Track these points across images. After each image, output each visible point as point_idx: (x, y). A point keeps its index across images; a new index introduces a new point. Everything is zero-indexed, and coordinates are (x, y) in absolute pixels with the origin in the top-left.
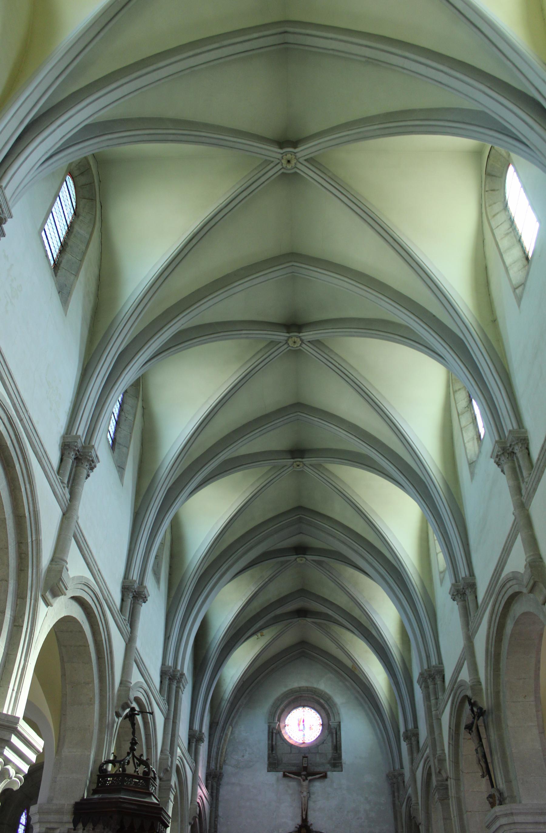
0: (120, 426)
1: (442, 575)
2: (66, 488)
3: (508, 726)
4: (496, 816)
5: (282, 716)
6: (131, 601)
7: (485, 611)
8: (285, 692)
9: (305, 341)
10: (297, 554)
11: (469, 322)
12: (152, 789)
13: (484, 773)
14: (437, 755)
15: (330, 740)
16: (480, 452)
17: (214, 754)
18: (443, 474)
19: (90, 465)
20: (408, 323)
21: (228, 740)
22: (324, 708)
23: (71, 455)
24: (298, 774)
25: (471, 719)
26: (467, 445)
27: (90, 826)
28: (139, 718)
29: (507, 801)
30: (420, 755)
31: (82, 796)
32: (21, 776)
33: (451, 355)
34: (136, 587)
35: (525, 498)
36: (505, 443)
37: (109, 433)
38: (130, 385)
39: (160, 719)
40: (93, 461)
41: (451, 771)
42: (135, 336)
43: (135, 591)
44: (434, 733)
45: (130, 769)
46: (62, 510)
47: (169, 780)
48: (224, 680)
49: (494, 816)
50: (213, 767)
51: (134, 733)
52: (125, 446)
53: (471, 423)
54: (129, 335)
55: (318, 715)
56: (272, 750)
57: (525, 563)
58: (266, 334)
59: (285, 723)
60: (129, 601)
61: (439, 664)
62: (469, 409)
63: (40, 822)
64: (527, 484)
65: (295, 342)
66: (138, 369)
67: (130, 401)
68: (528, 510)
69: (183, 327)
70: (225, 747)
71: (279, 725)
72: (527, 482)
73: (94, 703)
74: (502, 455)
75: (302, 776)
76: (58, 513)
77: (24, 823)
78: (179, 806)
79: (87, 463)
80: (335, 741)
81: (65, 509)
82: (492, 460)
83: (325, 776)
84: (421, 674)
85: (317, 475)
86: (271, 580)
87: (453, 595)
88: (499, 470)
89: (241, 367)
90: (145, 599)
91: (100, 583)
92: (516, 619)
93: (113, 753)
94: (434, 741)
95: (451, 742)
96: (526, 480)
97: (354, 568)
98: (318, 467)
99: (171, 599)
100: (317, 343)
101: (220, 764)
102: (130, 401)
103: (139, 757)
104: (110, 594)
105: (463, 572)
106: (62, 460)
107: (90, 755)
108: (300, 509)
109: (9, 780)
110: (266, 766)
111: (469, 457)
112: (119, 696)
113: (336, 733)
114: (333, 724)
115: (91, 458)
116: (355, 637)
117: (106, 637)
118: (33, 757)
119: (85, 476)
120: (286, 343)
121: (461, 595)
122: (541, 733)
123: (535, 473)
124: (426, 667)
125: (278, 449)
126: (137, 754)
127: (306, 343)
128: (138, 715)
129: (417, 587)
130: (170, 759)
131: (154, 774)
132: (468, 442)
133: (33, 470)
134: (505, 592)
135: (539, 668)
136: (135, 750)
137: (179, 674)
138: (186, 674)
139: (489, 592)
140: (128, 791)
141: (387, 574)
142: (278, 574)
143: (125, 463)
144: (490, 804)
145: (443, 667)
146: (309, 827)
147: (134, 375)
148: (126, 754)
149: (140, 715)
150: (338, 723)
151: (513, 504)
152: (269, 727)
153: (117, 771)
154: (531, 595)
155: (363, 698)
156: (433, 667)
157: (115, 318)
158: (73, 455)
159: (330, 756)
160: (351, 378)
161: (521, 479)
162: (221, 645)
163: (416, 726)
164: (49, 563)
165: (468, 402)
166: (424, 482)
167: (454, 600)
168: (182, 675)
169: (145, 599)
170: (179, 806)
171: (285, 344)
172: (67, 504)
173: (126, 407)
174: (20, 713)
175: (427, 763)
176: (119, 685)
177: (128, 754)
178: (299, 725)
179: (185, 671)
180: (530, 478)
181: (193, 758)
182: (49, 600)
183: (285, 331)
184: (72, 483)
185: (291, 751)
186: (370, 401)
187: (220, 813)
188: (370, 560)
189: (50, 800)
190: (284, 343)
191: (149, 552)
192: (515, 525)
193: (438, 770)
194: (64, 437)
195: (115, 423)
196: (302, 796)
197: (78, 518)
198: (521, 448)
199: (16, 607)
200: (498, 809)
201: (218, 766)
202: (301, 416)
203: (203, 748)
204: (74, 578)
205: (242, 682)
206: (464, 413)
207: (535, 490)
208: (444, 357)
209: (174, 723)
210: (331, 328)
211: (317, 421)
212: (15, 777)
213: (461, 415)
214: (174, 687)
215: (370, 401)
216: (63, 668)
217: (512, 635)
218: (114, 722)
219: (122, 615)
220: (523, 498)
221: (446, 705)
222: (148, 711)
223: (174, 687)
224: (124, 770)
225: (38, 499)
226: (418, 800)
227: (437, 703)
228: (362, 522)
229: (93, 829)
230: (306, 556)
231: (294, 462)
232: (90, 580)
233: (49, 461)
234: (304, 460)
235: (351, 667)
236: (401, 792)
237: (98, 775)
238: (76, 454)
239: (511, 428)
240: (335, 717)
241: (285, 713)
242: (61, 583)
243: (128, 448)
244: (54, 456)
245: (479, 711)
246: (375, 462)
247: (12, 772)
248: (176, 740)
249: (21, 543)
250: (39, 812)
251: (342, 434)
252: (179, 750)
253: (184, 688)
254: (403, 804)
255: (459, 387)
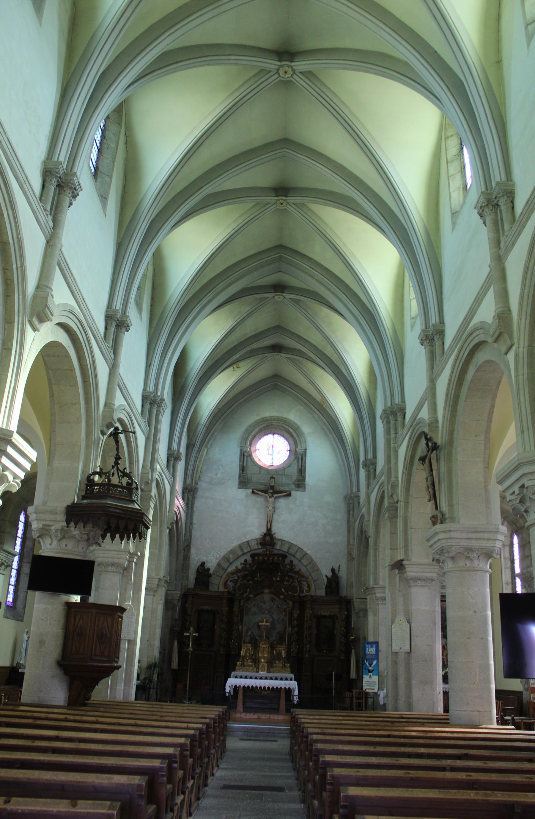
0: (102, 154)
1: (413, 320)
2: (49, 216)
3: (457, 460)
4: (436, 532)
5: (254, 441)
6: (115, 329)
7: (450, 356)
8: (257, 420)
9: (296, 72)
10: (275, 292)
11: (472, 61)
12: (135, 497)
13: (430, 497)
14: (391, 482)
15: (296, 465)
16: (464, 202)
17: (190, 471)
18: (425, 223)
19: (73, 193)
20: (407, 58)
21: (203, 460)
22: (292, 436)
23: (53, 182)
24: (266, 492)
25: (425, 453)
26: (452, 194)
27: (81, 525)
28: (122, 437)
29: (447, 521)
30: (376, 480)
31: (73, 501)
32: (19, 481)
33: (448, 98)
34: (119, 316)
35: (503, 251)
36: (491, 194)
37: (91, 161)
38: (113, 109)
39: (141, 439)
40: (75, 189)
41: (402, 495)
42: (117, 55)
43: (118, 320)
44: (390, 463)
45: (115, 480)
46: (45, 237)
47: (150, 491)
48: (201, 407)
49: (434, 532)
50: (189, 483)
51: (117, 449)
52: (107, 175)
53: (459, 172)
54: (110, 53)
55: (286, 442)
56: (243, 471)
57: (494, 314)
58: (256, 61)
59: (255, 448)
60: (112, 330)
61: (402, 403)
62: (459, 157)
63: (37, 520)
64: (506, 238)
65: (286, 72)
66: (121, 93)
67: (112, 128)
68: (504, 264)
69: (169, 48)
70: (201, 466)
71: (250, 449)
72: (507, 236)
73: (81, 422)
74: (486, 207)
75: (269, 494)
76: (41, 241)
77: (23, 521)
78: (158, 513)
79: (70, 190)
80: (300, 465)
81: (49, 237)
82: (476, 211)
83: (289, 495)
84: (384, 411)
85: (300, 215)
86: (249, 315)
87: (422, 340)
88: (482, 221)
89: (229, 96)
90: (128, 328)
91: (85, 311)
92: (478, 365)
93: (99, 466)
94: (390, 469)
95: (405, 471)
96: (506, 234)
97: (330, 308)
98: (301, 206)
99: (153, 330)
100: (308, 74)
101: (196, 481)
102: (112, 128)
103: (123, 471)
104: (94, 322)
105: (434, 319)
106: (43, 187)
107: (78, 467)
108: (281, 247)
109: (8, 484)
110: (237, 484)
111: (452, 207)
112: (104, 416)
113: (302, 459)
114: (300, 450)
115: (74, 185)
116: (326, 374)
117: (91, 362)
118: (28, 466)
119: (68, 204)
120: (277, 72)
121: (429, 340)
122: (486, 468)
123: (516, 228)
124: (389, 404)
125: (263, 186)
126: (121, 467)
127: (298, 74)
128: (121, 433)
129: (389, 331)
130: (150, 474)
131: (137, 485)
132: (454, 191)
133: (14, 195)
134: (472, 340)
135: (493, 412)
136: (119, 464)
137: (159, 400)
138: (166, 400)
139: (456, 340)
140: (113, 498)
141: (361, 315)
142: (255, 311)
143: (108, 193)
144: (433, 523)
145: (405, 405)
146: (273, 535)
147: (116, 99)
148: (111, 468)
149: (123, 434)
150: (304, 450)
151: (491, 257)
152: (241, 450)
153: (103, 481)
154: (495, 345)
155: (329, 429)
156: (396, 405)
157: (95, 34)
158: (55, 182)
159: (295, 478)
160: (342, 116)
161: (501, 232)
162: (199, 374)
163: (375, 456)
164: (34, 289)
165: (459, 150)
166: (406, 229)
167: (422, 345)
168: (162, 400)
169: (128, 328)
170: (158, 513)
171: (275, 74)
172: (50, 232)
173: (108, 134)
174: (14, 427)
175: (381, 488)
176: (103, 406)
177: (113, 467)
178: (268, 450)
179: (165, 397)
180: (510, 232)
181: (171, 473)
182: (35, 325)
183: (277, 59)
184: (55, 212)
185: (260, 472)
186: (359, 141)
187: (195, 520)
188: (345, 301)
189: (45, 503)
190: (275, 72)
191: (132, 282)
192: (489, 277)
193: (390, 494)
194: (45, 163)
195: (97, 150)
196: (268, 510)
197: (62, 246)
198: (506, 201)
199: (5, 331)
200: (438, 527)
201: (194, 482)
202: (287, 152)
203: (181, 466)
204: (59, 305)
205: (218, 410)
206: (454, 161)
207: (514, 244)
208: (440, 99)
209: (155, 442)
210: (325, 58)
211: (304, 159)
212: (13, 481)
213: (450, 163)
214: (155, 411)
215: (359, 141)
216: (51, 390)
217: (472, 380)
218: (99, 439)
219: (106, 343)
220: (501, 251)
221: (404, 439)
222: (130, 431)
223: (155, 411)
224: (109, 480)
225: (21, 226)
226: (370, 518)
227: (396, 437)
228: (341, 264)
229: (84, 527)
230: (283, 294)
231: (277, 200)
232: (75, 308)
233: (31, 187)
234: (287, 198)
235: (319, 401)
236: (356, 511)
237: (86, 484)
238: (58, 181)
239: (499, 180)
240: (302, 445)
241: (256, 439)
242: (47, 309)
243: (111, 177)
244: (36, 183)
245: (433, 445)
246: (358, 204)
247: (10, 477)
248: (156, 458)
249: (7, 269)
250: (36, 512)
251: (328, 174)
252: (158, 467)
253: (164, 412)
254: (356, 520)
255: (452, 134)
